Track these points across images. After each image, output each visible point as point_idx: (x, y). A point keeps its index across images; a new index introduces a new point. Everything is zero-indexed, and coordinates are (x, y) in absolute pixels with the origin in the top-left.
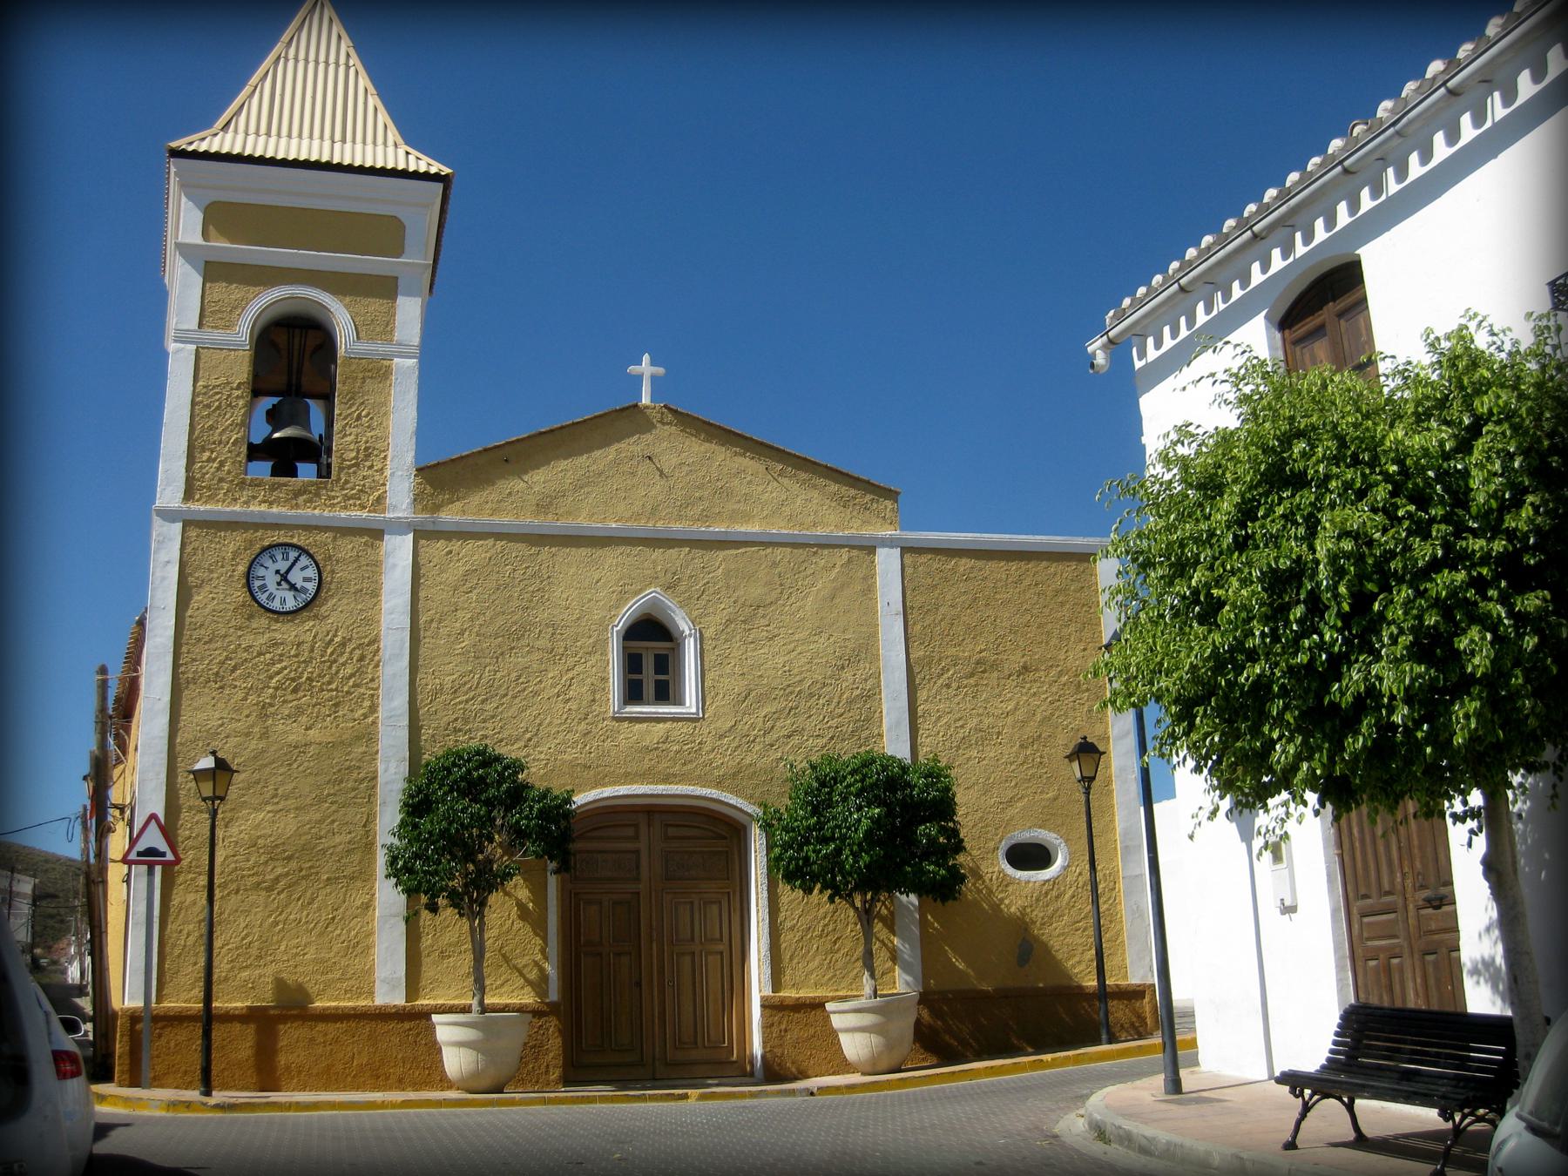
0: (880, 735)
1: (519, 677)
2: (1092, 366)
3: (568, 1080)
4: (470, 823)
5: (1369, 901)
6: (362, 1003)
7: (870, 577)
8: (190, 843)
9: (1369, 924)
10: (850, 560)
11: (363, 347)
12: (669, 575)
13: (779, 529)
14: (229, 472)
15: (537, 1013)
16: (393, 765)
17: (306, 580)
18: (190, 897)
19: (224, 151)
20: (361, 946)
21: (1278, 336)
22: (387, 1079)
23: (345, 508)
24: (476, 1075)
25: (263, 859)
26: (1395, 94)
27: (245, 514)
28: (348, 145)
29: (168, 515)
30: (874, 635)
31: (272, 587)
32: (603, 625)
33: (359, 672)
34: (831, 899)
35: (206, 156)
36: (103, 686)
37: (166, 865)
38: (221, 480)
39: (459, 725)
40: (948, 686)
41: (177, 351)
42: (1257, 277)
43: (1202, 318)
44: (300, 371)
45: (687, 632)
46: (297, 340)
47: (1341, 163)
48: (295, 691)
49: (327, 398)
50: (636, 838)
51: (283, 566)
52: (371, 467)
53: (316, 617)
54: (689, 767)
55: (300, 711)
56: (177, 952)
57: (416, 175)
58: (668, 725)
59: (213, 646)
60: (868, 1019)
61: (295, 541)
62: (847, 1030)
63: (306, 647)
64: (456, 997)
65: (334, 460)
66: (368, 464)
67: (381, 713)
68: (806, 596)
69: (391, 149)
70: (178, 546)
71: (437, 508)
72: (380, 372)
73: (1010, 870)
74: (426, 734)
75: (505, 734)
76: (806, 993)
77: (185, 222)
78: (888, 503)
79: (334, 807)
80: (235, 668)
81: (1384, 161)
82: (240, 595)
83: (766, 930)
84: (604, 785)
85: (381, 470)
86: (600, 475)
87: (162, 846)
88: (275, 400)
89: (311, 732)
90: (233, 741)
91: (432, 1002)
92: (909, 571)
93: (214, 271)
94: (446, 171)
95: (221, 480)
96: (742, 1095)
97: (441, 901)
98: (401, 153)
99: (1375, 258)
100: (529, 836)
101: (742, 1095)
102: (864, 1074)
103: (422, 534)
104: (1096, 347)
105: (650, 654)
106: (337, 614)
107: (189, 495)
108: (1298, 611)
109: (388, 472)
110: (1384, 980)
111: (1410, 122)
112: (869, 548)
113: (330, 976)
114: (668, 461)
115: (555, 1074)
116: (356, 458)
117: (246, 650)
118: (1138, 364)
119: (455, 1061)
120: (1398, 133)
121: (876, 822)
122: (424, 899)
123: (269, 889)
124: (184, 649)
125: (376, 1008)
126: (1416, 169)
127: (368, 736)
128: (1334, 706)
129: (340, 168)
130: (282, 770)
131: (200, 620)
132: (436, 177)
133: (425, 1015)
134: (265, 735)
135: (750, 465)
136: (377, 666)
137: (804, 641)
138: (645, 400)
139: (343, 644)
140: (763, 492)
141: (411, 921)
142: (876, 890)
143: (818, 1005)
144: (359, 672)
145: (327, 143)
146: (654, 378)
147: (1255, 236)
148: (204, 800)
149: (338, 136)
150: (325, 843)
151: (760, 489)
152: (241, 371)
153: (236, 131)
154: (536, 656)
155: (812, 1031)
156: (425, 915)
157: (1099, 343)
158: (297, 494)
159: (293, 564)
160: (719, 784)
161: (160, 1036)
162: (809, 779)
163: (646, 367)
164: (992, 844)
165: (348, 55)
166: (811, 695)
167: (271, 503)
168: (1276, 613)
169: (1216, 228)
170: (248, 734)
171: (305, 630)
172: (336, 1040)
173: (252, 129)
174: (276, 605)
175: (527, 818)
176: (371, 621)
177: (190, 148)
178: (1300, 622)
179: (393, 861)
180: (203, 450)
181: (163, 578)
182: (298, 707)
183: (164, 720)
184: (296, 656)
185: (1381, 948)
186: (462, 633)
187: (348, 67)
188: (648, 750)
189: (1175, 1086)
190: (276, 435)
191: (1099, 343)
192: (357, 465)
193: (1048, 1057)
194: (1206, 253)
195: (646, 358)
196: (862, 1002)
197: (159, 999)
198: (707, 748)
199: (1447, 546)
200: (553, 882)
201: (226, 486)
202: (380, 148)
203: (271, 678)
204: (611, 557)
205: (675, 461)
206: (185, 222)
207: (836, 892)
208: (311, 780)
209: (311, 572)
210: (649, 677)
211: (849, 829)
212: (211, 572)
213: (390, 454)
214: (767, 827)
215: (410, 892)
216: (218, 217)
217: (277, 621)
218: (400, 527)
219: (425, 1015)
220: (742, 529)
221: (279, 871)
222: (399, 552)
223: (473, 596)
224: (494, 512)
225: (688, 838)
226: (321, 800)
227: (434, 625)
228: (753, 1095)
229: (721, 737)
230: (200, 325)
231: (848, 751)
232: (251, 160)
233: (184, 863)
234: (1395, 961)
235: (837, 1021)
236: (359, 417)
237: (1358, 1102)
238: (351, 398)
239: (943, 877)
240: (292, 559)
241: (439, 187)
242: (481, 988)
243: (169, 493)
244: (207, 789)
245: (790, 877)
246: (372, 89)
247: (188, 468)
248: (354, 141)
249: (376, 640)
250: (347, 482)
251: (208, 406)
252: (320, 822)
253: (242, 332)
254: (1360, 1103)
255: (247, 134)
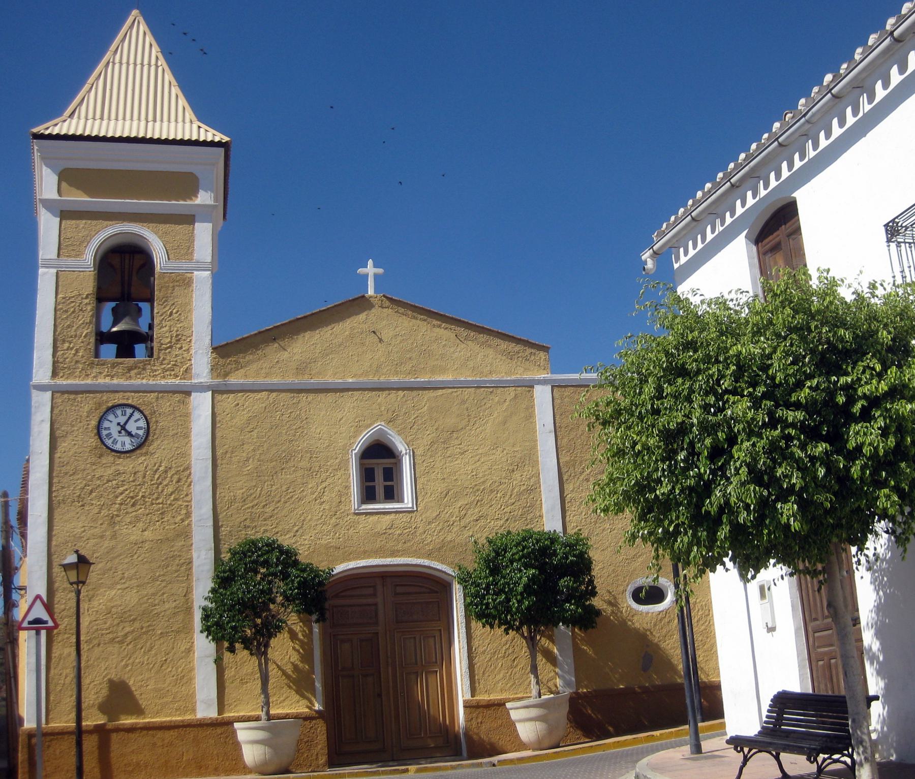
0: (541, 516)
1: (288, 488)
2: (644, 269)
3: (333, 762)
4: (259, 592)
5: (818, 623)
6: (188, 717)
7: (531, 407)
8: (65, 613)
9: (819, 637)
10: (516, 396)
11: (173, 264)
12: (390, 413)
13: (465, 376)
14: (83, 357)
15: (307, 718)
16: (203, 553)
17: (138, 428)
18: (65, 650)
19: (70, 133)
20: (186, 678)
21: (754, 248)
22: (207, 768)
23: (164, 377)
24: (265, 763)
25: (116, 622)
26: (807, 95)
27: (95, 385)
28: (158, 124)
29: (41, 388)
30: (536, 445)
31: (115, 434)
32: (346, 449)
33: (177, 490)
34: (506, 632)
35: (58, 137)
36: (6, 505)
37: (49, 630)
38: (77, 362)
39: (248, 523)
40: (587, 480)
41: (44, 274)
42: (739, 210)
43: (710, 236)
44: (130, 285)
45: (404, 452)
46: (127, 261)
47: (777, 139)
48: (133, 505)
49: (150, 300)
50: (374, 595)
51: (122, 420)
52: (181, 348)
53: (146, 454)
54: (409, 544)
55: (138, 519)
56: (59, 688)
57: (205, 144)
58: (393, 516)
59: (76, 477)
60: (534, 712)
61: (130, 402)
62: (520, 721)
63: (140, 475)
64: (252, 710)
65: (155, 344)
66: (178, 346)
67: (194, 518)
68: (487, 422)
69: (188, 125)
70: (49, 409)
71: (226, 375)
72: (186, 282)
73: (635, 605)
74: (224, 531)
75: (280, 528)
76: (494, 697)
77: (47, 184)
78: (542, 354)
79: (164, 584)
80: (91, 492)
81: (806, 136)
82: (93, 441)
83: (466, 655)
84: (350, 560)
85: (188, 350)
86: (340, 345)
87: (45, 616)
88: (113, 304)
89: (146, 533)
90: (92, 542)
91: (236, 714)
92: (557, 401)
93: (66, 214)
94: (226, 139)
95: (77, 362)
96: (446, 768)
97: (237, 645)
98: (195, 127)
99: (804, 197)
100: (294, 600)
101: (446, 768)
102: (534, 750)
103: (216, 391)
104: (646, 255)
105: (379, 468)
106: (160, 450)
107: (54, 374)
108: (681, 456)
109: (192, 352)
110: (827, 673)
111: (814, 115)
112: (530, 386)
113: (165, 700)
114: (386, 335)
115: (323, 760)
116: (170, 342)
117: (99, 478)
118: (676, 266)
119: (251, 754)
120: (807, 121)
121: (532, 580)
122: (226, 644)
123: (121, 642)
124: (55, 480)
125: (198, 720)
126: (823, 143)
127: (185, 534)
128: (708, 513)
129: (152, 141)
130: (126, 560)
131: (66, 459)
132: (219, 144)
133: (229, 723)
134: (114, 536)
135: (445, 333)
136: (190, 485)
137: (486, 454)
138: (371, 292)
139: (166, 472)
140: (454, 352)
141: (218, 661)
142: (537, 623)
143: (501, 704)
144: (177, 490)
145: (143, 123)
146: (376, 276)
147: (732, 185)
148: (72, 584)
149: (150, 117)
150: (158, 609)
151: (452, 350)
152: (88, 285)
153: (79, 118)
154: (300, 473)
155: (500, 722)
156: (227, 655)
157: (648, 254)
158: (130, 369)
159: (129, 418)
160: (429, 556)
161: (49, 747)
162: (487, 550)
163: (370, 269)
164: (621, 588)
165: (157, 58)
166: (492, 491)
167: (112, 377)
168: (670, 455)
169: (712, 179)
170: (102, 537)
171: (138, 463)
172: (171, 744)
173: (90, 115)
174: (118, 447)
175: (290, 589)
176: (186, 455)
177: (47, 132)
178: (685, 460)
179: (206, 617)
180: (64, 341)
181: (40, 432)
182: (136, 517)
183: (44, 530)
184: (134, 481)
185: (825, 653)
186: (248, 460)
187: (157, 67)
188: (379, 534)
189: (697, 749)
190: (115, 329)
191: (648, 254)
192: (171, 347)
193: (657, 733)
194: (710, 193)
195: (370, 262)
196: (532, 701)
197: (47, 722)
198: (421, 530)
199: (771, 414)
200: (316, 629)
201: (80, 366)
202: (180, 125)
203: (117, 497)
204: (349, 402)
205: (391, 334)
206: (47, 184)
207: (509, 627)
208: (147, 566)
209: (142, 423)
210: (380, 484)
211: (515, 584)
212: (73, 426)
213: (194, 338)
214: (462, 581)
215: (218, 640)
216: (67, 177)
217: (119, 458)
218: (202, 388)
219: (229, 723)
220: (440, 379)
221: (128, 629)
222: (202, 404)
223: (255, 434)
224: (267, 375)
225: (409, 593)
226: (155, 579)
227: (228, 455)
228: (453, 768)
229: (430, 523)
230: (59, 255)
231: (517, 527)
232: (89, 138)
233: (61, 627)
234: (833, 661)
235: (514, 715)
236: (171, 314)
237: (782, 754)
238: (166, 299)
239: (580, 614)
240: (128, 415)
241: (222, 151)
242: (267, 703)
243: (41, 373)
244: (74, 578)
245: (479, 616)
246: (174, 82)
247: (54, 355)
248: (162, 120)
249: (188, 468)
250: (164, 359)
251: (66, 311)
252: (153, 594)
253: (89, 257)
254: (783, 756)
255: (87, 119)
